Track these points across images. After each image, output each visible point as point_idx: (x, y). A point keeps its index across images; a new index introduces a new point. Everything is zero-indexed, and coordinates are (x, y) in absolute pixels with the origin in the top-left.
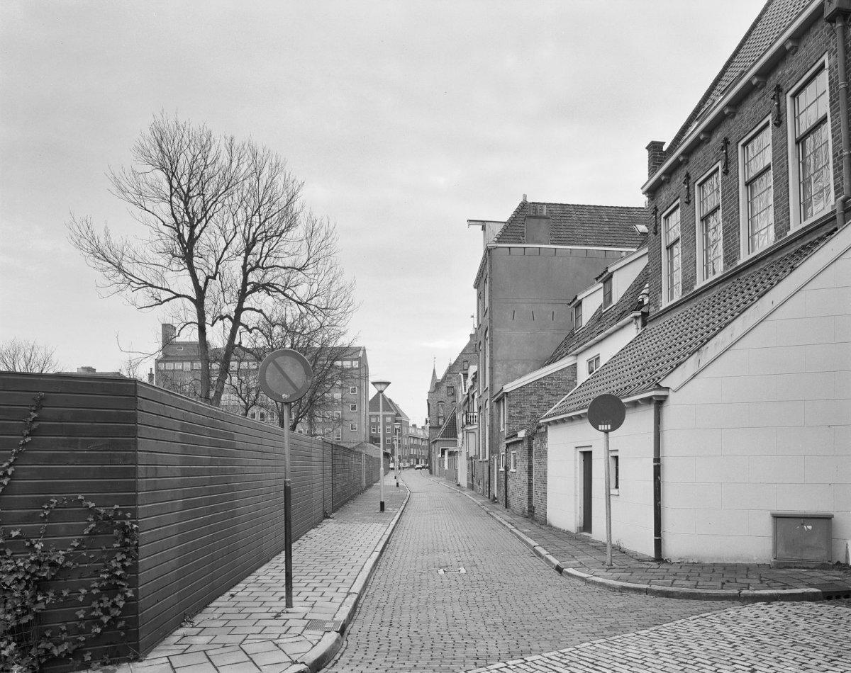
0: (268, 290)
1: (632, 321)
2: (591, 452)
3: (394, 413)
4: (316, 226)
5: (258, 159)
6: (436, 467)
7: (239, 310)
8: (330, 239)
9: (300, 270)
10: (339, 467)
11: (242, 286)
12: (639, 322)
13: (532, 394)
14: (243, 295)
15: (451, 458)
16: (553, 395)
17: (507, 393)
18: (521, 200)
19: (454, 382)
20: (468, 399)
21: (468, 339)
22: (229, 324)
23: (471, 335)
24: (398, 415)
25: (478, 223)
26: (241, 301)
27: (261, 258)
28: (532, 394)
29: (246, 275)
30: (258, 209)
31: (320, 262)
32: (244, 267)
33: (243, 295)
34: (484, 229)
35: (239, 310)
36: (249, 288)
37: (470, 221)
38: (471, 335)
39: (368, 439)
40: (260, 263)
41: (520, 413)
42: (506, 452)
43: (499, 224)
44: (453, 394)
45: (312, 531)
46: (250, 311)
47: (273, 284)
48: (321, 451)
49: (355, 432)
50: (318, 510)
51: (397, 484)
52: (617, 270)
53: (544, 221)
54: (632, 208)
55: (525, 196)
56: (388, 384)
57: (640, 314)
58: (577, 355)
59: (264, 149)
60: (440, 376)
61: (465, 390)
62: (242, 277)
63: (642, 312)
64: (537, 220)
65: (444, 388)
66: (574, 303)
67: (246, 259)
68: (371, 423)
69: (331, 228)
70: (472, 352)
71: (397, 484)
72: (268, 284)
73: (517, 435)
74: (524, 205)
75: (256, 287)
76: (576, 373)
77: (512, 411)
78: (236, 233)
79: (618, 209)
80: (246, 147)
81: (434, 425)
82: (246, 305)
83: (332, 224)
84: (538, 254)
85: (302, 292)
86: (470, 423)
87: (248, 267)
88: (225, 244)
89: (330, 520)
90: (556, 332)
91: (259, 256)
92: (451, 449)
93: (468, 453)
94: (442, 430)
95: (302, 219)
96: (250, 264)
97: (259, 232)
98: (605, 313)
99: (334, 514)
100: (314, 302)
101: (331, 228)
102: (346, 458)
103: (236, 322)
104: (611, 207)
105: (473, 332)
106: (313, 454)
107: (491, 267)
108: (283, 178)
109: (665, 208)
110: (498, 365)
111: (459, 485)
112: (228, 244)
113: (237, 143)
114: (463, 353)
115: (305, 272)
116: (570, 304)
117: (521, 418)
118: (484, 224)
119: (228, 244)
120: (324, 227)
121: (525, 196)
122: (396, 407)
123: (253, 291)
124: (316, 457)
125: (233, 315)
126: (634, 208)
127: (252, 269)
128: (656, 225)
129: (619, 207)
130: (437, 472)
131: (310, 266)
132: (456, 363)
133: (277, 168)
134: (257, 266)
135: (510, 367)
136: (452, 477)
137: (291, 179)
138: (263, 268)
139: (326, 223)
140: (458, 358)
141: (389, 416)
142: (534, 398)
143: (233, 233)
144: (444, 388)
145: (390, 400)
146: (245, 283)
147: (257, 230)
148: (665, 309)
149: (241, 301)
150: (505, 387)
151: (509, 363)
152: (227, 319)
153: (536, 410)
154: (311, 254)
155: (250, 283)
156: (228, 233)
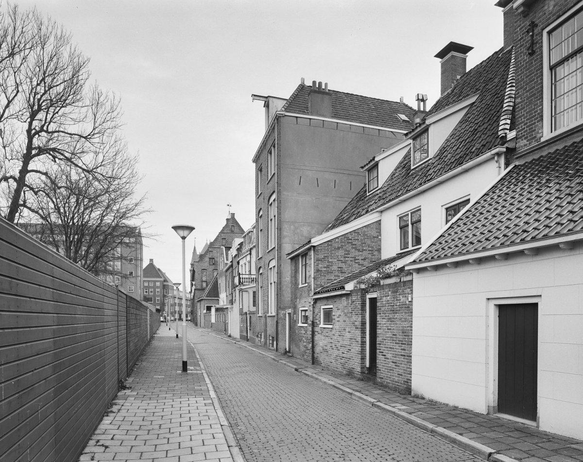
0: (54, 157)
1: (494, 158)
2: (536, 305)
3: (162, 279)
4: (101, 99)
5: (43, 28)
6: (201, 319)
7: (24, 171)
8: (115, 113)
9: (86, 138)
10: (132, 322)
11: (27, 150)
12: (502, 160)
13: (339, 248)
14: (27, 158)
15: (217, 313)
16: (359, 250)
17: (314, 247)
18: (300, 83)
19: (215, 254)
20: (232, 266)
21: (225, 223)
22: (14, 185)
23: (227, 219)
24: (165, 281)
25: (261, 99)
26: (26, 163)
27: (45, 123)
28: (339, 248)
29: (30, 138)
30: (43, 79)
31: (106, 134)
32: (29, 131)
33: (27, 158)
34: (267, 105)
35: (24, 171)
36: (34, 152)
37: (255, 95)
38: (227, 219)
39: (142, 298)
40: (45, 128)
41: (328, 267)
42: (314, 307)
43: (283, 101)
44: (214, 264)
45: (106, 421)
46: (34, 173)
47: (59, 150)
48: (115, 302)
49: (135, 289)
50: (111, 381)
51: (177, 335)
52: (434, 123)
53: (327, 97)
54: (391, 102)
55: (303, 80)
56: (191, 229)
57: (505, 150)
58: (381, 212)
59: (49, 20)
60: (199, 251)
61: (227, 260)
62: (27, 141)
63: (507, 148)
64: (320, 95)
65: (207, 259)
66: (369, 165)
67: (30, 124)
68: (145, 287)
69: (116, 102)
70: (229, 232)
71: (177, 335)
72: (54, 150)
73: (343, 288)
74: (302, 88)
75: (41, 151)
76: (380, 231)
77: (320, 266)
78: (18, 92)
79: (380, 101)
80: (30, 16)
81: (199, 287)
82: (30, 167)
83: (117, 99)
84: (322, 126)
85: (88, 160)
86: (242, 283)
87: (33, 131)
88: (6, 102)
89: (128, 392)
90: (338, 199)
91: (43, 122)
92: (218, 306)
93: (241, 310)
94: (207, 291)
95: (87, 92)
96: (34, 129)
97: (44, 98)
98: (413, 170)
99: (130, 380)
100: (99, 170)
101: (116, 102)
102: (138, 312)
103: (21, 182)
104: (374, 99)
105: (229, 217)
106: (106, 306)
107: (279, 134)
108: (68, 49)
109: (555, 17)
110: (285, 227)
111: (230, 336)
112: (9, 102)
113: (20, 10)
114: (222, 232)
115: (92, 140)
116: (362, 167)
117: (328, 273)
118: (267, 101)
119: (9, 102)
120: (109, 101)
121: (303, 80)
122: (163, 275)
123: (38, 155)
124: (109, 311)
125: (17, 175)
126: (392, 102)
127: (37, 133)
128: (533, 43)
129: (381, 100)
130: (202, 324)
131: (96, 136)
132: (216, 240)
133: (62, 40)
134: (42, 130)
135: (296, 228)
136: (223, 329)
137: (77, 53)
138: (47, 132)
139: (111, 96)
140: (218, 236)
141: (158, 281)
142: (341, 253)
143: (15, 92)
144: (207, 259)
145: (159, 269)
146: (30, 147)
147: (42, 96)
148: (547, 141)
149: (26, 163)
150: (312, 241)
151: (296, 225)
152: (11, 181)
153: (343, 265)
154: (97, 125)
155: (35, 148)
156: (10, 90)
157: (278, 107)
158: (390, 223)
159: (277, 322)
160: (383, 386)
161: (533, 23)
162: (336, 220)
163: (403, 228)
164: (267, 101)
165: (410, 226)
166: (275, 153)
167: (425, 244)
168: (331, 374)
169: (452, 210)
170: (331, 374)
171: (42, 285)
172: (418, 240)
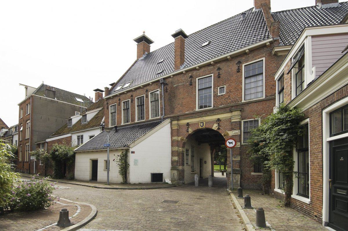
17: (47, 142)
18: (42, 83)
58: (72, 134)
74: (43, 86)
157: (31, 92)
158: (75, 137)
159: (30, 164)
160: (130, 184)
161: (108, 103)
162: (57, 132)
163: (78, 139)
164: (26, 88)
165: (80, 139)
166: (30, 106)
167: (84, 143)
168: (167, 81)
169: (91, 137)
170: (167, 81)
171: (103, 189)
172: (82, 142)
